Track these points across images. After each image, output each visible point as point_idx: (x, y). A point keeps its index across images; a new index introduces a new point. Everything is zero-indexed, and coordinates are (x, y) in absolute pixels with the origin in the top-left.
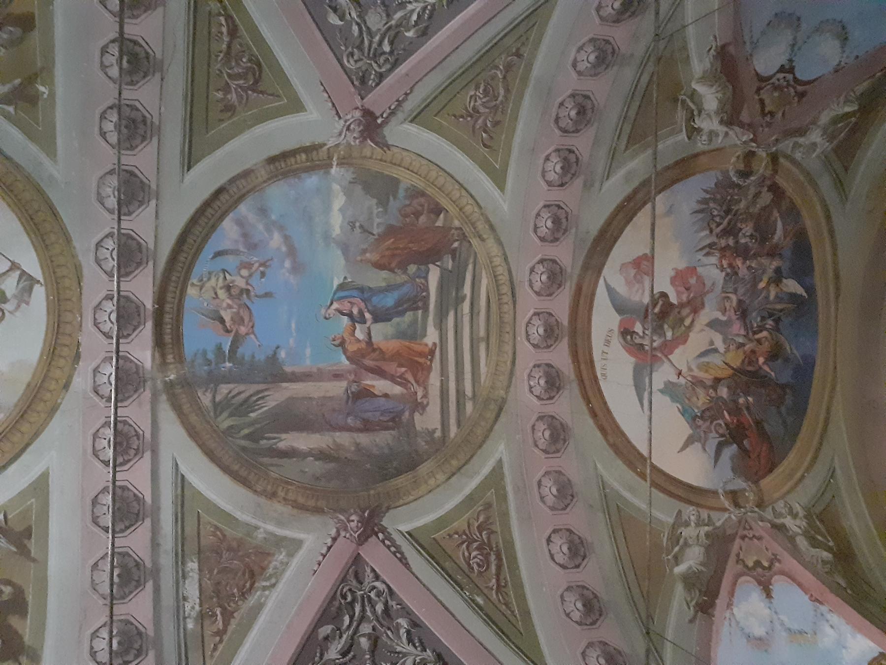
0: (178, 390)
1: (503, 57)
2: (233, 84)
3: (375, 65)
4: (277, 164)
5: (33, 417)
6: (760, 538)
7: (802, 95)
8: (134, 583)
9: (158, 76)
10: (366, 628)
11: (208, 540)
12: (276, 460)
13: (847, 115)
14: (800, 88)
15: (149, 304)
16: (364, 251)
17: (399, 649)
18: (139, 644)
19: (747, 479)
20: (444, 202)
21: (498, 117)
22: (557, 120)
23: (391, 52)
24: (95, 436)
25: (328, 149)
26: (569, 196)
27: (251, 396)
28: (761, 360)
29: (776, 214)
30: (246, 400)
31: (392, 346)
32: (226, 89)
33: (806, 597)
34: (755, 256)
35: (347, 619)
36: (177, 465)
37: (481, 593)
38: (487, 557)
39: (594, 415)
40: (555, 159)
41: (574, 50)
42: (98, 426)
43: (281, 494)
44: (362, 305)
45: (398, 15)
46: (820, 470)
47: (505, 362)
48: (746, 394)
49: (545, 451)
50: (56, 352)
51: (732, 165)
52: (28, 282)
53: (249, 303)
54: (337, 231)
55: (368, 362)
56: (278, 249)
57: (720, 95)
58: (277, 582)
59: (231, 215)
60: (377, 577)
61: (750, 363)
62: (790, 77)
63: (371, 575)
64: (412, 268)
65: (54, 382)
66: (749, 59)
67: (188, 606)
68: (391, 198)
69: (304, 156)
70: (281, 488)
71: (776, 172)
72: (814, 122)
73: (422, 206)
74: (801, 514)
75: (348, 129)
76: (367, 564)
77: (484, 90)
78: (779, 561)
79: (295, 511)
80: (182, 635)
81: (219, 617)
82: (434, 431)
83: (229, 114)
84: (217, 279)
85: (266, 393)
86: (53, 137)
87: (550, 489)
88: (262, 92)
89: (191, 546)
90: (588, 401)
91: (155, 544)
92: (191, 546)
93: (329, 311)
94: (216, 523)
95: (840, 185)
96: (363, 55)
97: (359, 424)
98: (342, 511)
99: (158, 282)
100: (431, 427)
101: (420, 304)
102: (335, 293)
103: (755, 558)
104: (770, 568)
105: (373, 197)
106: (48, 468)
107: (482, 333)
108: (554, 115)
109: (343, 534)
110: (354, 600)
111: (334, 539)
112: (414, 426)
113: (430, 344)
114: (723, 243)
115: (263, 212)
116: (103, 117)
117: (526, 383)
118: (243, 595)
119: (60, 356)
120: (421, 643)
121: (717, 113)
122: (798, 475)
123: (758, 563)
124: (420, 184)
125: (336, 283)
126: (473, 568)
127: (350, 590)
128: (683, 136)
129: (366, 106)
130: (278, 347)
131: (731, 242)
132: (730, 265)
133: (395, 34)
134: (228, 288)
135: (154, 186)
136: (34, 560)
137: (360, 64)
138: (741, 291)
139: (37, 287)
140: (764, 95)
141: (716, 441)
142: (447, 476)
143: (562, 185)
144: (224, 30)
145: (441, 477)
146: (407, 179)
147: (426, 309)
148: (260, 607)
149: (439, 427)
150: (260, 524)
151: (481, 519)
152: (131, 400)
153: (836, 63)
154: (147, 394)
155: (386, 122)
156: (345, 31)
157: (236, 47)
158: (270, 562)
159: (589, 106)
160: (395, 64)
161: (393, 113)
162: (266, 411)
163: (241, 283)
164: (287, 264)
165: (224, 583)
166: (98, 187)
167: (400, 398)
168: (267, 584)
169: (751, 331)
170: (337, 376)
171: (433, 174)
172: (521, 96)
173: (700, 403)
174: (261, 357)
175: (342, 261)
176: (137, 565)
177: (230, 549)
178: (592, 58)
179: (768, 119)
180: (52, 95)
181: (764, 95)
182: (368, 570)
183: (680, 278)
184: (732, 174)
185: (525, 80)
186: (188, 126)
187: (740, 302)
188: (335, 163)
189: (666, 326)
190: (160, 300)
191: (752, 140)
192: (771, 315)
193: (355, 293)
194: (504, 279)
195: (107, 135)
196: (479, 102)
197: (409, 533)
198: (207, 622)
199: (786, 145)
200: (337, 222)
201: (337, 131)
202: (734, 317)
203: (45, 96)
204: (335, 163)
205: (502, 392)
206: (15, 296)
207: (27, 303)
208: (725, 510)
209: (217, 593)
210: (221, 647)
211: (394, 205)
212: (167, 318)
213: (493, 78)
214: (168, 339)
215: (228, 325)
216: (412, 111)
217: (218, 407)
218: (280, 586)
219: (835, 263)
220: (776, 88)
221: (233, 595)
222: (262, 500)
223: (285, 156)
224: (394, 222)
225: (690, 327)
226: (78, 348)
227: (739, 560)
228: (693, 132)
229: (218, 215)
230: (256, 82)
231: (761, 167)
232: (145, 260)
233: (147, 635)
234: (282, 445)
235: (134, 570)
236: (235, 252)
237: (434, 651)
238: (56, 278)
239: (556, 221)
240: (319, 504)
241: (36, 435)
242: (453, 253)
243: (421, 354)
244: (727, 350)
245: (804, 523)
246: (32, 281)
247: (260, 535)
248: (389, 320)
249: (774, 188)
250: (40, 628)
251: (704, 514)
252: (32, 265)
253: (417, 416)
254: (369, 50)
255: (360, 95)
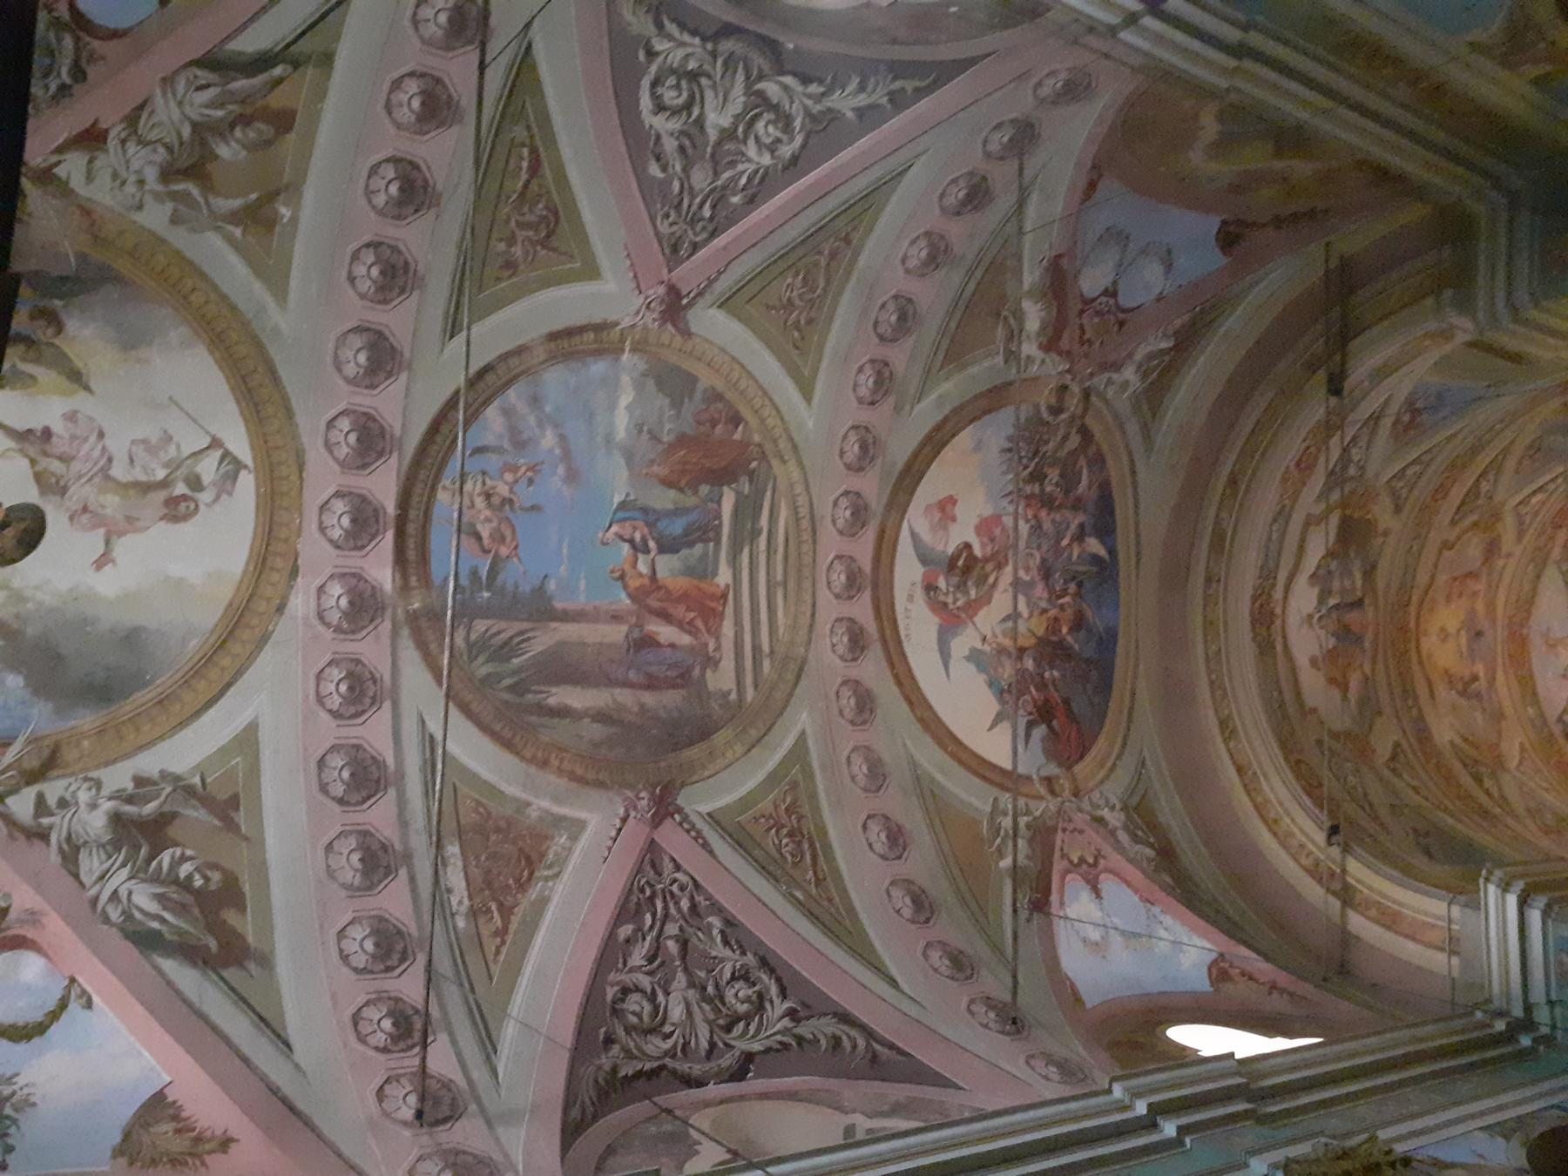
0: (424, 623)
1: (832, 240)
2: (521, 234)
3: (690, 233)
4: (559, 341)
5: (235, 648)
6: (1081, 832)
7: (1121, 324)
8: (382, 870)
9: (433, 211)
10: (672, 929)
11: (469, 818)
12: (545, 720)
13: (1162, 352)
14: (1121, 316)
15: (391, 509)
16: (652, 462)
17: (714, 953)
18: (402, 945)
19: (1060, 765)
20: (746, 413)
21: (813, 314)
22: (876, 324)
23: (712, 218)
24: (319, 676)
25: (623, 329)
26: (878, 418)
27: (511, 638)
28: (1065, 630)
29: (1082, 462)
30: (506, 644)
31: (680, 583)
32: (511, 241)
33: (1136, 898)
34: (1060, 507)
35: (648, 918)
36: (423, 722)
37: (800, 887)
38: (799, 843)
39: (899, 683)
40: (868, 371)
41: (906, 243)
42: (321, 665)
43: (555, 762)
44: (646, 530)
45: (726, 175)
46: (1129, 762)
47: (805, 613)
48: (1052, 668)
49: (852, 723)
50: (269, 563)
51: (1045, 398)
52: (230, 467)
53: (511, 516)
54: (621, 433)
55: (653, 603)
56: (551, 450)
57: (1043, 313)
58: (560, 872)
59: (496, 403)
60: (678, 868)
61: (1054, 633)
62: (1112, 301)
63: (671, 865)
64: (704, 489)
65: (264, 603)
66: (1076, 276)
67: (454, 901)
68: (686, 400)
69: (592, 335)
70: (553, 755)
71: (1086, 410)
72: (1130, 355)
73: (720, 412)
74: (1118, 806)
75: (648, 307)
76: (666, 853)
77: (804, 278)
78: (1104, 857)
79: (574, 785)
80: (453, 938)
81: (496, 914)
82: (729, 693)
83: (509, 273)
84: (475, 485)
85: (530, 634)
86: (287, 276)
87: (860, 768)
88: (554, 250)
89: (449, 825)
90: (892, 665)
91: (404, 823)
92: (449, 825)
93: (608, 535)
94: (477, 796)
95: (1147, 435)
96: (680, 216)
97: (641, 679)
98: (631, 787)
99: (403, 478)
100: (725, 688)
101: (711, 534)
102: (615, 513)
103: (1079, 854)
104: (1095, 864)
105: (667, 395)
106: (256, 718)
107: (779, 577)
108: (873, 317)
109: (633, 814)
110: (653, 895)
111: (624, 820)
112: (706, 686)
113: (722, 585)
114: (1028, 489)
115: (535, 401)
116: (355, 256)
117: (828, 640)
118: (522, 886)
119: (272, 568)
120: (741, 947)
121: (1038, 334)
122: (1109, 764)
123: (1082, 860)
124: (720, 386)
125: (617, 499)
126: (786, 858)
127: (647, 882)
128: (1000, 359)
129: (674, 281)
130: (546, 576)
131: (1037, 490)
132: (1035, 516)
133: (718, 198)
134: (488, 496)
135: (407, 354)
136: (246, 839)
137: (675, 228)
138: (1045, 548)
139: (243, 474)
140: (1085, 321)
141: (1025, 720)
142: (746, 747)
143: (872, 403)
144: (525, 164)
145: (739, 749)
146: (706, 379)
147: (718, 542)
148: (543, 902)
149: (734, 687)
150: (531, 799)
151: (788, 800)
152: (364, 633)
153: (1157, 291)
154: (387, 625)
155: (690, 305)
156: (665, 185)
157: (534, 186)
158: (548, 848)
159: (911, 311)
160: (714, 234)
161: (700, 294)
162: (530, 658)
163: (503, 490)
164: (561, 470)
165: (495, 872)
166: (337, 348)
167: (691, 649)
168: (550, 873)
169: (1054, 596)
170: (616, 618)
171: (735, 375)
172: (840, 293)
173: (1006, 676)
174: (526, 588)
175: (625, 473)
176: (384, 847)
177: (498, 830)
178: (924, 254)
179: (1086, 346)
180: (294, 220)
181: (1085, 321)
182: (667, 859)
183: (986, 527)
184: (1043, 409)
185: (848, 274)
186: (457, 282)
187: (1043, 561)
188: (627, 349)
189: (970, 583)
190: (404, 504)
191: (1068, 371)
192: (1074, 578)
193: (637, 514)
194: (804, 511)
195: (357, 281)
196: (795, 293)
197: (709, 814)
198: (482, 920)
199: (1100, 381)
200: (622, 423)
201: (636, 308)
202: (1037, 578)
203: (285, 220)
204: (627, 349)
205: (802, 650)
206: (214, 483)
207: (230, 494)
208: (1041, 798)
209: (489, 884)
210: (504, 950)
211: (689, 408)
212: (411, 528)
213: (816, 264)
214: (411, 554)
215: (486, 541)
216: (722, 294)
217: (474, 649)
218: (565, 877)
219: (1137, 524)
220: (1099, 313)
221: (508, 886)
222: (533, 770)
223: (569, 333)
224: (688, 431)
225: (994, 585)
226: (296, 560)
227: (1063, 856)
228: (1011, 356)
229: (481, 400)
230: (548, 236)
231: (1073, 403)
232: (388, 449)
233: (409, 935)
234: (552, 701)
235: (380, 853)
236: (498, 450)
237: (755, 954)
238: (271, 464)
239: (864, 447)
240: (601, 777)
241: (239, 673)
242: (751, 475)
243: (713, 597)
244: (1031, 616)
245: (1122, 816)
246: (238, 465)
247: (534, 813)
248: (678, 552)
249: (1086, 434)
250: (267, 928)
251: (1021, 802)
252: (240, 445)
253: (709, 673)
254: (688, 213)
255: (668, 266)
